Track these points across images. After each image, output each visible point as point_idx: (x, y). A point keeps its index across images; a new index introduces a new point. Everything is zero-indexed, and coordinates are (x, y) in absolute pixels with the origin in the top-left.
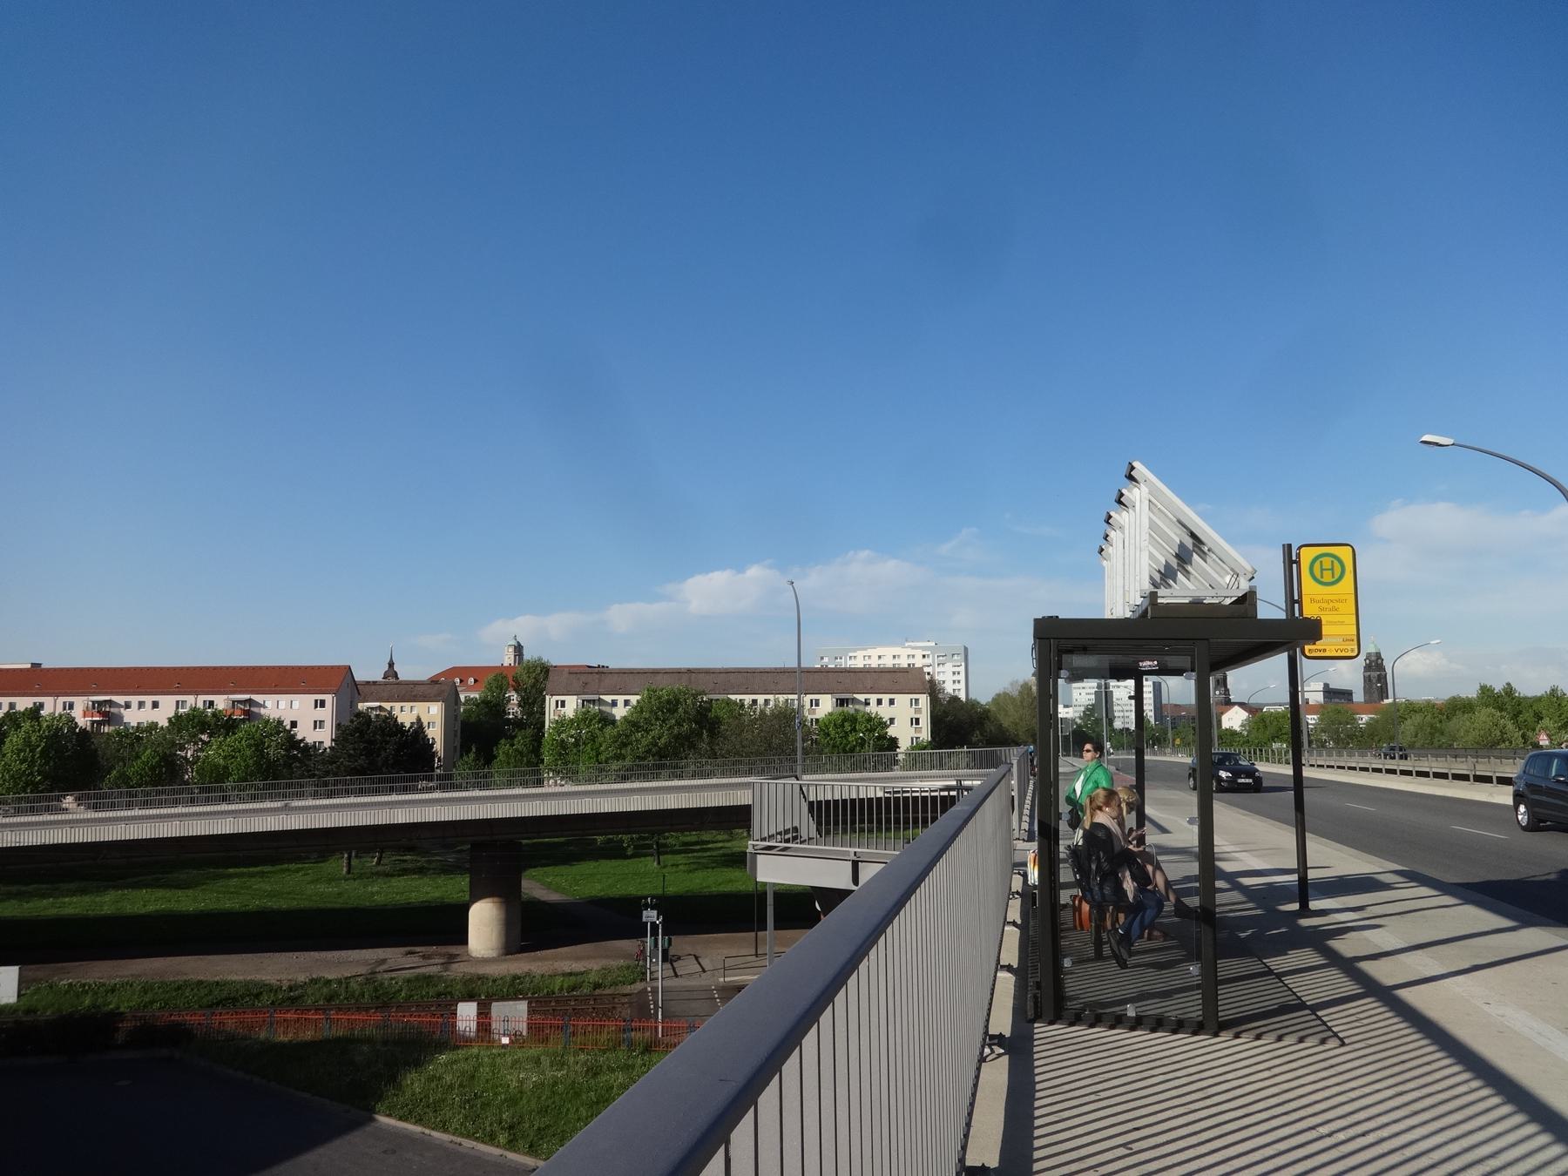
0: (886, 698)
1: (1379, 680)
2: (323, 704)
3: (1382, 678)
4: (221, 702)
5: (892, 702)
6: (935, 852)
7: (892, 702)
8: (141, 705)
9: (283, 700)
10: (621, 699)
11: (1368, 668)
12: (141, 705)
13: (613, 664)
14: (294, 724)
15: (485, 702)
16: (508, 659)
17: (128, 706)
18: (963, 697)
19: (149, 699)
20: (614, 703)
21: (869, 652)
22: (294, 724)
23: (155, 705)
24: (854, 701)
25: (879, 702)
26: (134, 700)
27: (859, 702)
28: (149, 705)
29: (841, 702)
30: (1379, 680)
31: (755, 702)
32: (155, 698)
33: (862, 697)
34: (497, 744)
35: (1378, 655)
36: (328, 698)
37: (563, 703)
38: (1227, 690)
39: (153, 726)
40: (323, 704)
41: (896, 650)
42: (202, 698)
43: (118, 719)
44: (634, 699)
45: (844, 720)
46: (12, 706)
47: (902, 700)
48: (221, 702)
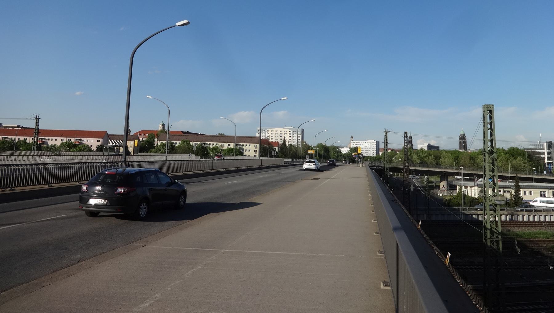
0: (248, 144)
2: (99, 141)
4: (73, 140)
5: (56, 140)
6: (105, 218)
7: (250, 145)
8: (52, 140)
9: (89, 140)
10: (212, 143)
11: (460, 139)
12: (52, 140)
14: (91, 146)
15: (148, 141)
16: (160, 128)
17: (49, 140)
19: (54, 138)
20: (210, 144)
22: (91, 146)
23: (56, 140)
24: (240, 145)
26: (50, 138)
28: (54, 140)
29: (236, 145)
31: (15, 139)
33: (242, 144)
34: (263, 140)
35: (464, 135)
36: (101, 140)
39: (55, 145)
40: (99, 141)
41: (281, 129)
42: (68, 138)
43: (46, 143)
46: (19, 139)
47: (252, 145)
48: (73, 140)
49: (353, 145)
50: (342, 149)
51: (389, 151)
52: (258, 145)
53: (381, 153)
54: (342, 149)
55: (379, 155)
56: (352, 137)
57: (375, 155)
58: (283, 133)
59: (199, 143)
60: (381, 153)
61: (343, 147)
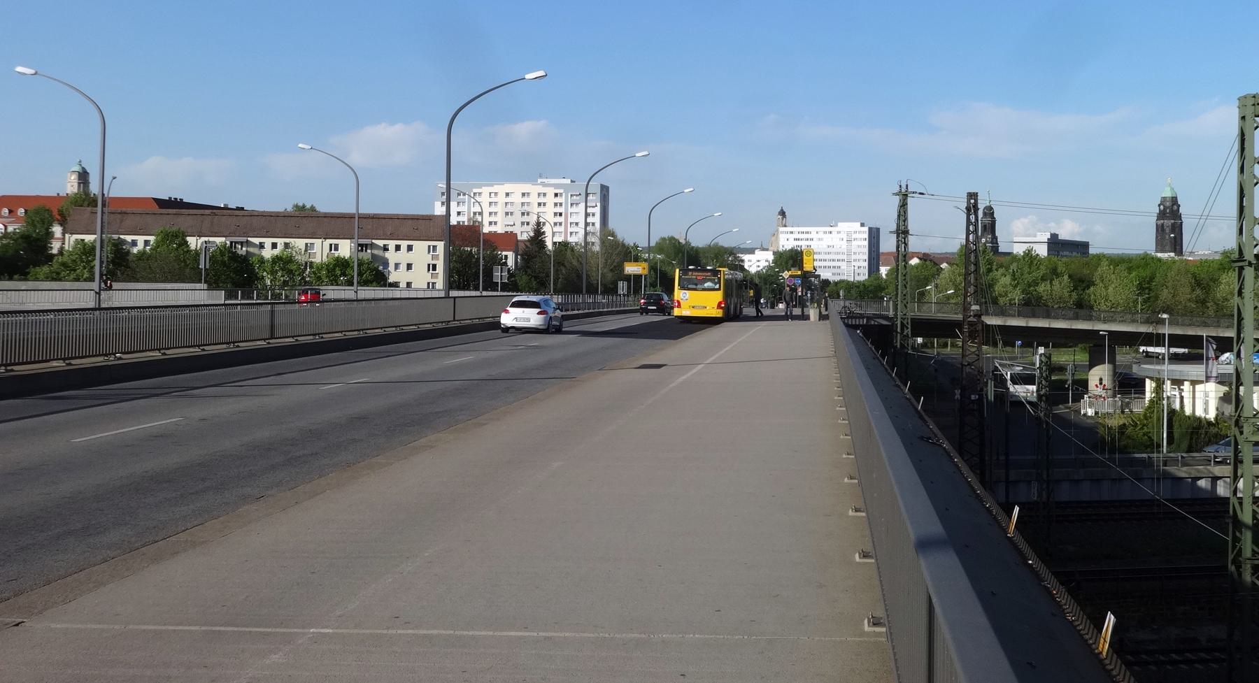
1: (1173, 231)
3: (1178, 229)
5: (410, 248)
7: (410, 248)
10: (268, 242)
11: (1162, 215)
13: (322, 208)
15: (25, 237)
18: (683, 241)
20: (262, 246)
21: (495, 188)
24: (373, 246)
25: (398, 248)
27: (378, 247)
29: (362, 247)
30: (1173, 231)
32: (410, 243)
33: (380, 243)
35: (1174, 200)
37: (435, 247)
38: (995, 238)
41: (526, 187)
44: (152, 238)
45: (335, 266)
47: (421, 246)
49: (787, 241)
50: (746, 257)
51: (914, 261)
52: (440, 245)
53: (884, 271)
54: (746, 257)
55: (879, 277)
56: (783, 213)
57: (863, 276)
58: (534, 199)
59: (219, 240)
60: (884, 271)
61: (751, 251)
